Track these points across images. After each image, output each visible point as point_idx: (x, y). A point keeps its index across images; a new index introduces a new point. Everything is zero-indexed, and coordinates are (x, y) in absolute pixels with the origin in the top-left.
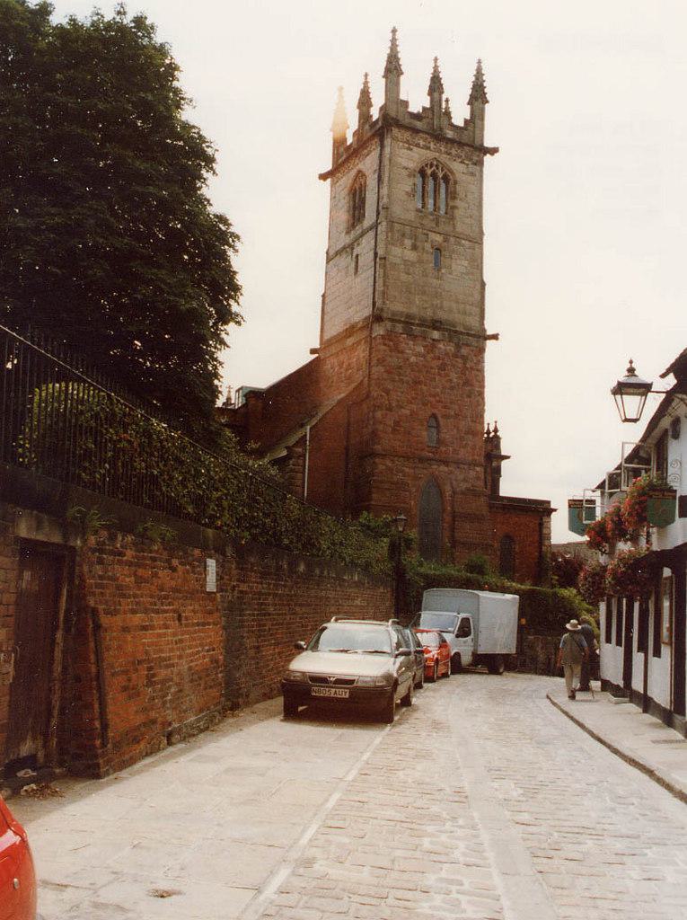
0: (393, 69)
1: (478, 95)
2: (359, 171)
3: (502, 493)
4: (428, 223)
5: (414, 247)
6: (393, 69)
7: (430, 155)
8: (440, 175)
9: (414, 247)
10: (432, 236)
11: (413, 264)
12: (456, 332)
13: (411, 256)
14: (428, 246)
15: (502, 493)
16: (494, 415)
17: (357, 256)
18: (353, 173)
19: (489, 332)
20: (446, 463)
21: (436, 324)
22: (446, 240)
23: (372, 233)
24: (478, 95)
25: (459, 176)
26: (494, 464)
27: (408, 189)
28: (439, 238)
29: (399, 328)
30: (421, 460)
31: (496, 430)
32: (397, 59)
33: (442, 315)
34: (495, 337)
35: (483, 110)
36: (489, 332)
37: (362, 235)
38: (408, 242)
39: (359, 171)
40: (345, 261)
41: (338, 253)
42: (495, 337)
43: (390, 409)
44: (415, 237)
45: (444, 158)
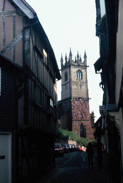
0: (71, 55)
1: (85, 56)
2: (66, 71)
3: (102, 105)
4: (78, 81)
5: (76, 86)
6: (71, 55)
7: (78, 69)
8: (80, 72)
9: (76, 86)
10: (79, 83)
11: (76, 88)
12: (84, 99)
13: (76, 87)
14: (78, 85)
15: (102, 105)
16: (97, 39)
17: (67, 87)
18: (65, 71)
19: (89, 98)
20: (84, 121)
21: (80, 98)
22: (81, 83)
23: (69, 83)
24: (85, 56)
25: (83, 72)
26: (93, 118)
27: (74, 76)
28: (80, 83)
29: (75, 99)
30: (80, 120)
31: (93, 112)
32: (71, 53)
33: (81, 96)
34: (91, 99)
35: (86, 59)
36: (89, 98)
37: (67, 83)
38: (75, 85)
39: (66, 71)
40: (64, 87)
41: (63, 85)
42: (91, 99)
43: (74, 113)
44: (76, 84)
45: (80, 69)
